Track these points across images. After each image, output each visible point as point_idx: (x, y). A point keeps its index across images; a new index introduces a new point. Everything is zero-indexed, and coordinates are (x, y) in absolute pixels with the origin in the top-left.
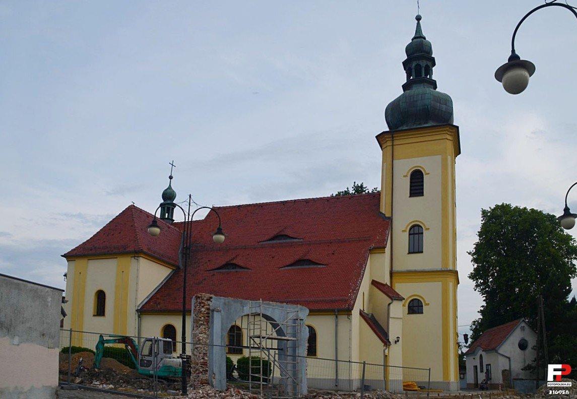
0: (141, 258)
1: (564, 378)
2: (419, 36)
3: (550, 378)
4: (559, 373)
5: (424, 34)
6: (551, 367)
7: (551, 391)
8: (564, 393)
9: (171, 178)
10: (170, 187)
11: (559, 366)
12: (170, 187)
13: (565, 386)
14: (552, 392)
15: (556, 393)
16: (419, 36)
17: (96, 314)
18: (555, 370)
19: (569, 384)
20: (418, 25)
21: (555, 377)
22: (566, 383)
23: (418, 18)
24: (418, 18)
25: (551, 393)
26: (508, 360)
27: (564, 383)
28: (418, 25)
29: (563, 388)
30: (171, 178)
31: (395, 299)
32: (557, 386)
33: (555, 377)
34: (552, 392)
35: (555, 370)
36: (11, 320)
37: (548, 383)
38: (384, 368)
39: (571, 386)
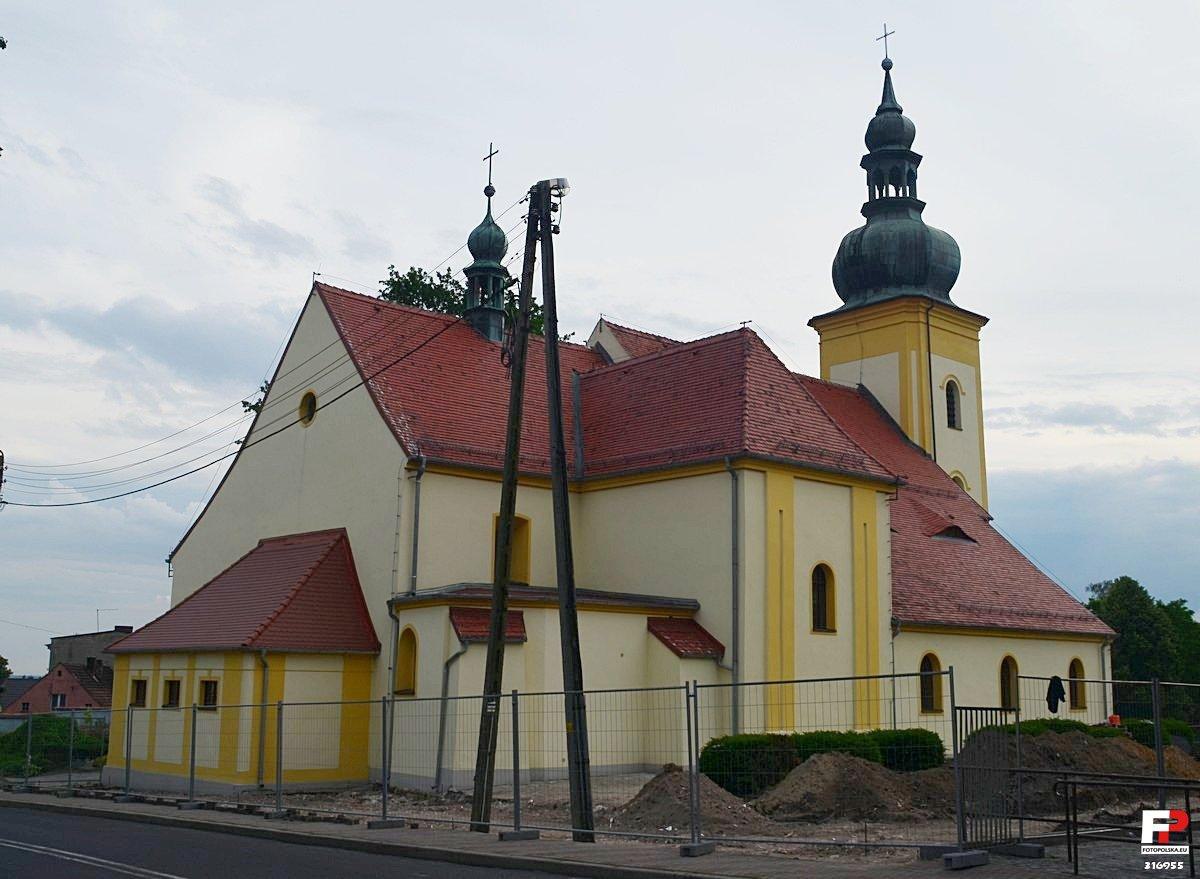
0: (746, 472)
1: (1174, 837)
2: (889, 107)
3: (1147, 837)
4: (1165, 828)
5: (900, 101)
6: (1148, 816)
7: (1148, 864)
8: (1174, 867)
9: (489, 191)
10: (488, 221)
11: (1165, 814)
12: (488, 221)
13: (1176, 853)
14: (1151, 866)
15: (1159, 866)
16: (889, 107)
17: (167, 703)
18: (1158, 821)
19: (1184, 850)
20: (888, 76)
21: (1156, 835)
22: (1179, 847)
23: (887, 65)
24: (887, 65)
25: (1147, 867)
26: (453, 668)
27: (1175, 847)
28: (888, 76)
29: (1171, 858)
30: (489, 191)
31: (471, 643)
32: (1160, 853)
33: (1156, 835)
34: (1151, 866)
35: (1158, 821)
36: (52, 685)
37: (1143, 847)
38: (442, 703)
39: (1187, 853)
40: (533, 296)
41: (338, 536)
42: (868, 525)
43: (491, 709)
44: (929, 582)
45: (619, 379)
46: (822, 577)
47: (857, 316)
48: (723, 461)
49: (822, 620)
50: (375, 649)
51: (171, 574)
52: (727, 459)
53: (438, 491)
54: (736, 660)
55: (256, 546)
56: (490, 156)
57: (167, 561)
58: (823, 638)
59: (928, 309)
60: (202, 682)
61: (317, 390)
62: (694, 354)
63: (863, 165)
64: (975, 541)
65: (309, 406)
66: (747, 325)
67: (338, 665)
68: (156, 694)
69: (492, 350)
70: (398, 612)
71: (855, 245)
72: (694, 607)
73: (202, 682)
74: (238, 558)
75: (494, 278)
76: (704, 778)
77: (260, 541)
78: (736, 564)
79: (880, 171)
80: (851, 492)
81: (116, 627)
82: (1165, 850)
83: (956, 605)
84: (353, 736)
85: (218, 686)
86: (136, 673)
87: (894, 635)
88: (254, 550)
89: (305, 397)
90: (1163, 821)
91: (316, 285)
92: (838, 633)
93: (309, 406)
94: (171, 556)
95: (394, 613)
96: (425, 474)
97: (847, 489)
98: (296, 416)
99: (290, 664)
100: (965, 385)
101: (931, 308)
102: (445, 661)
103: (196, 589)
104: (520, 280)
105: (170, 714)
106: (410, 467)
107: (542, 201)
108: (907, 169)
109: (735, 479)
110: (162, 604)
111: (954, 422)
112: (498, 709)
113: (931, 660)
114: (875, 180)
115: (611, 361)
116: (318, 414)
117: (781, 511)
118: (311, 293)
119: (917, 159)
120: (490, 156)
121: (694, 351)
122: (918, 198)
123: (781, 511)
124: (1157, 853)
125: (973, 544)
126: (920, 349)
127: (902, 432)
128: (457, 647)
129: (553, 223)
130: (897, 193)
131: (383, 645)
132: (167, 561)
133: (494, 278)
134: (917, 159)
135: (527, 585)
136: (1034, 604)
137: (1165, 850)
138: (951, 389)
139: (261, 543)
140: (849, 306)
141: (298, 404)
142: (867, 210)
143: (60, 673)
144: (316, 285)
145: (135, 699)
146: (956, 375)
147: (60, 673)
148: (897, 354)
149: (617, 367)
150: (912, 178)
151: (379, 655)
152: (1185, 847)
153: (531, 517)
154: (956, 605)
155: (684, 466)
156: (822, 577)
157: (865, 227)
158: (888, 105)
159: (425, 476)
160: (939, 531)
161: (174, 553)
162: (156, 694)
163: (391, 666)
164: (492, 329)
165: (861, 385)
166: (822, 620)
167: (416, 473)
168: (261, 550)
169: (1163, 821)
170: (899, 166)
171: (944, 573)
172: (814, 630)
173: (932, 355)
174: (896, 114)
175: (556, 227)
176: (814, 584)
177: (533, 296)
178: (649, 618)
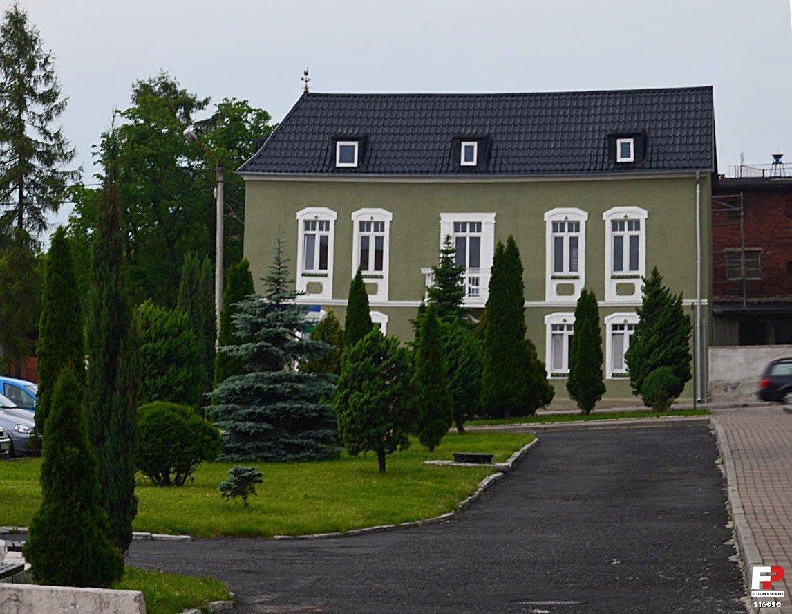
3: (755, 585)
4: (768, 579)
18: (762, 574)
19: (781, 594)
35: (762, 574)
37: (752, 592)
40: (604, 219)
76: (133, 557)
82: (768, 594)
85: (628, 267)
90: (767, 574)
107: (308, 68)
122: (646, 212)
124: (762, 596)
131: (525, 270)
137: (768, 594)
152: (782, 592)
169: (767, 574)
177: (604, 219)
178: (544, 300)
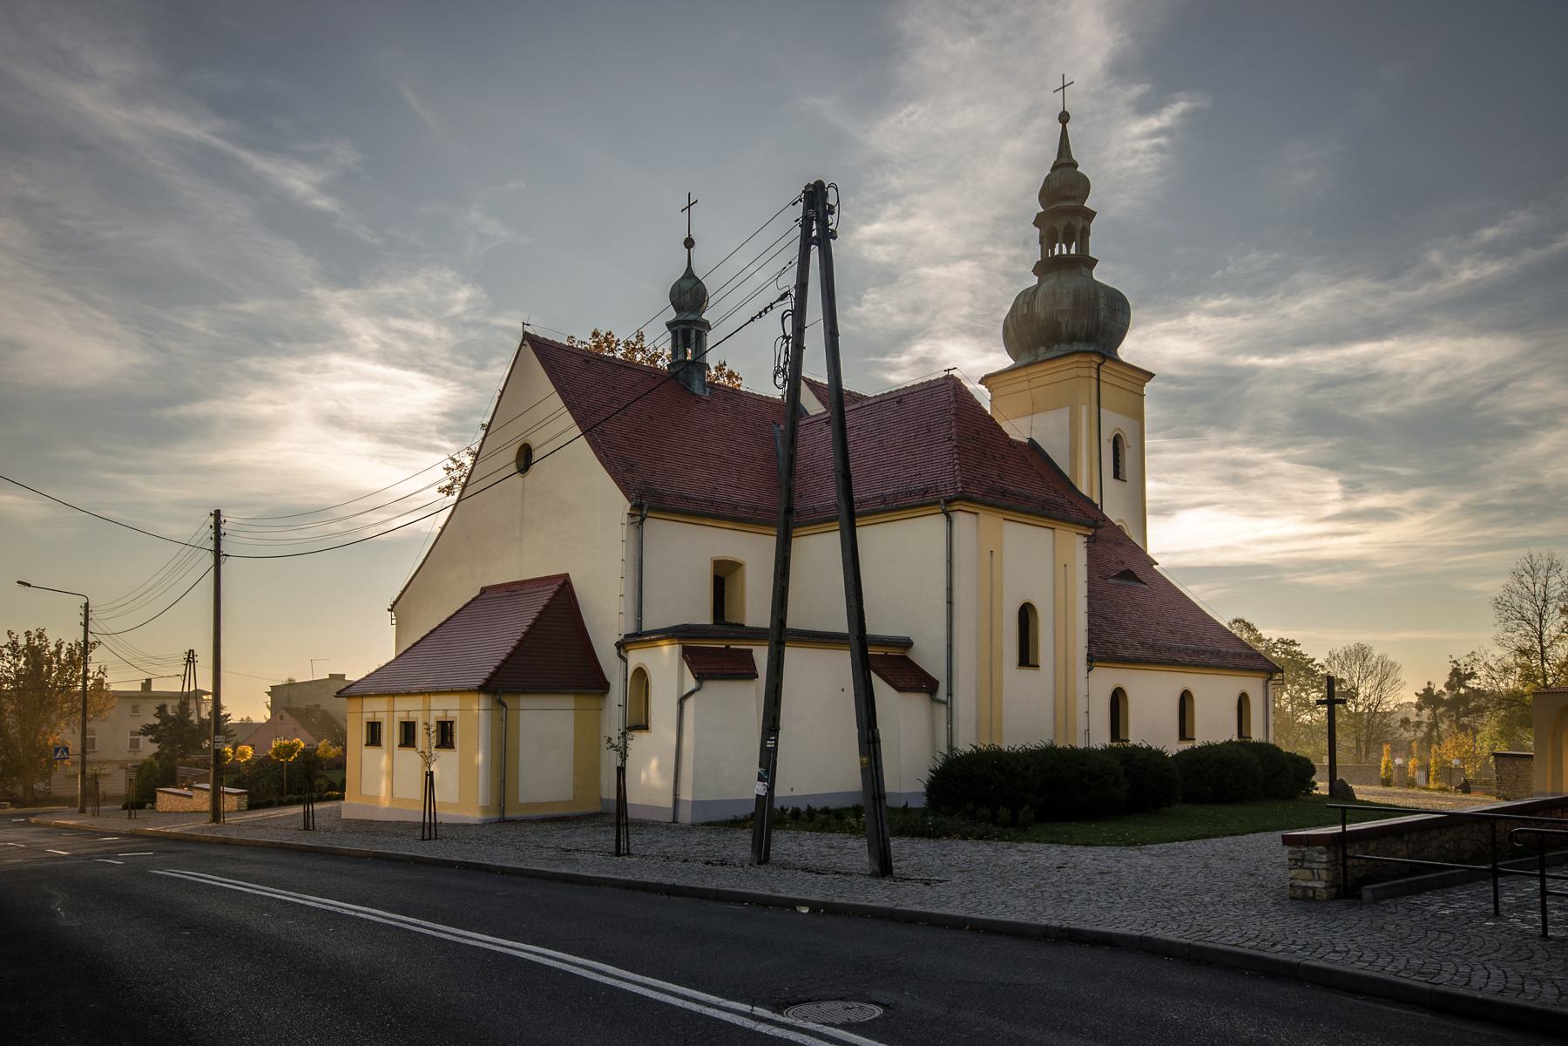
2: (1065, 161)
9: (689, 243)
10: (689, 274)
12: (689, 274)
16: (1065, 161)
20: (1064, 128)
28: (1064, 128)
30: (689, 243)
41: (561, 582)
42: (1068, 567)
43: (770, 744)
44: (1114, 622)
45: (821, 430)
46: (1026, 614)
47: (1029, 372)
48: (938, 503)
49: (1026, 658)
50: (602, 688)
51: (394, 622)
52: (942, 500)
53: (661, 531)
54: (950, 694)
55: (478, 593)
56: (689, 207)
57: (389, 610)
58: (1027, 673)
59: (1099, 365)
60: (368, 723)
61: (534, 441)
62: (898, 402)
63: (1036, 223)
64: (1145, 584)
65: (525, 459)
66: (951, 373)
67: (568, 702)
68: (391, 734)
69: (698, 402)
70: (627, 652)
71: (1028, 303)
72: (907, 644)
73: (368, 723)
74: (462, 605)
75: (697, 330)
77: (482, 589)
78: (950, 602)
79: (1055, 229)
80: (1054, 533)
81: (330, 675)
83: (1140, 643)
84: (586, 769)
86: (371, 715)
87: (1089, 670)
88: (477, 597)
89: (520, 449)
91: (526, 336)
92: (1041, 668)
93: (525, 459)
94: (393, 606)
95: (622, 653)
96: (647, 519)
97: (1050, 531)
98: (513, 468)
99: (526, 702)
100: (1129, 439)
101: (1102, 364)
102: (680, 696)
103: (423, 635)
104: (793, 293)
105: (444, 754)
106: (633, 512)
108: (1081, 225)
109: (950, 520)
110: (386, 652)
111: (1118, 473)
112: (776, 744)
113: (1119, 694)
114: (1047, 240)
115: (807, 412)
116: (533, 468)
117: (991, 552)
118: (522, 345)
119: (1091, 215)
120: (690, 205)
121: (898, 399)
122: (1090, 255)
123: (991, 552)
125: (1143, 586)
126: (1090, 405)
127: (1071, 483)
128: (690, 683)
129: (830, 227)
130: (1068, 250)
132: (389, 610)
133: (697, 330)
134: (1091, 215)
135: (743, 625)
136: (1205, 642)
138: (1117, 442)
139: (484, 591)
140: (1019, 363)
141: (513, 458)
142: (1039, 269)
143: (282, 717)
144: (526, 336)
145: (403, 740)
146: (1122, 429)
147: (282, 717)
148: (1068, 408)
149: (813, 419)
150: (1085, 233)
151: (607, 693)
153: (744, 560)
154: (1140, 643)
155: (898, 509)
156: (1026, 614)
157: (1037, 288)
158: (1065, 160)
159: (647, 521)
160: (1115, 574)
161: (395, 603)
162: (391, 734)
163: (621, 704)
164: (697, 381)
165: (1031, 439)
166: (1026, 658)
167: (639, 518)
168: (481, 597)
170: (1073, 223)
171: (1124, 614)
172: (1020, 665)
173: (1102, 410)
174: (1072, 169)
175: (834, 232)
176: (1019, 622)
